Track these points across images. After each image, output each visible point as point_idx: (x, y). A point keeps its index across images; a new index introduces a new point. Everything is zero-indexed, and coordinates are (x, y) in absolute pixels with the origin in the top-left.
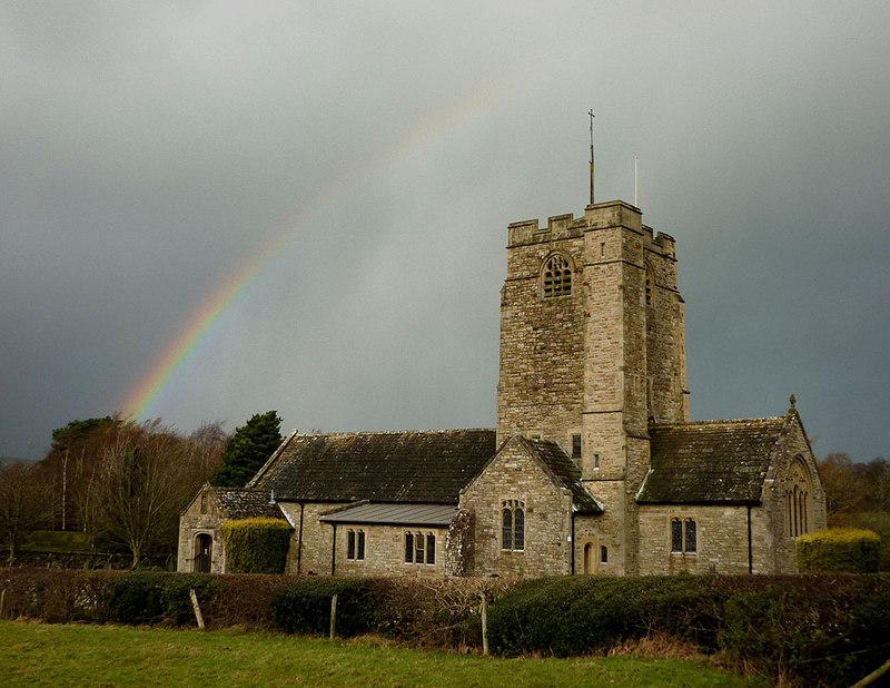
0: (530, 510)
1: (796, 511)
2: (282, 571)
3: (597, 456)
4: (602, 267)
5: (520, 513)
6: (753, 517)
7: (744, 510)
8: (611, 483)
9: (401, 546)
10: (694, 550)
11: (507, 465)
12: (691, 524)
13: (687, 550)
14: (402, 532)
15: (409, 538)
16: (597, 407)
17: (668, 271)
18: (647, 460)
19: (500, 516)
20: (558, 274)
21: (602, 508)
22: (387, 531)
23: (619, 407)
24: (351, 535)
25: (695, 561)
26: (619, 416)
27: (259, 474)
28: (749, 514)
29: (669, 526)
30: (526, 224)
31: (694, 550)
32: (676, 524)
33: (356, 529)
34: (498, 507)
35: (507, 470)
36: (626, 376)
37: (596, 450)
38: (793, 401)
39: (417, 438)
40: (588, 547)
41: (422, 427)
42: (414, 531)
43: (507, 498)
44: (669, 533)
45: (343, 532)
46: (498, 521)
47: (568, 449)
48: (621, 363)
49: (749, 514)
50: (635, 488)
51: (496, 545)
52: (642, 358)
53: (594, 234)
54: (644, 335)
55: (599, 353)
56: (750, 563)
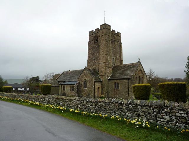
1: (140, 81)
2: (185, 85)
5: (86, 81)
6: (129, 82)
7: (127, 80)
9: (70, 88)
10: (118, 88)
14: (70, 86)
15: (71, 86)
16: (101, 62)
17: (119, 39)
18: (111, 72)
20: (96, 39)
22: (68, 86)
24: (63, 86)
28: (128, 81)
29: (114, 84)
33: (64, 85)
34: (83, 81)
37: (101, 70)
38: (139, 59)
39: (73, 71)
40: (99, 88)
41: (80, 69)
42: (71, 85)
43: (84, 79)
45: (62, 86)
46: (83, 83)
47: (97, 70)
49: (128, 81)
50: (108, 77)
51: (83, 87)
56: (128, 91)
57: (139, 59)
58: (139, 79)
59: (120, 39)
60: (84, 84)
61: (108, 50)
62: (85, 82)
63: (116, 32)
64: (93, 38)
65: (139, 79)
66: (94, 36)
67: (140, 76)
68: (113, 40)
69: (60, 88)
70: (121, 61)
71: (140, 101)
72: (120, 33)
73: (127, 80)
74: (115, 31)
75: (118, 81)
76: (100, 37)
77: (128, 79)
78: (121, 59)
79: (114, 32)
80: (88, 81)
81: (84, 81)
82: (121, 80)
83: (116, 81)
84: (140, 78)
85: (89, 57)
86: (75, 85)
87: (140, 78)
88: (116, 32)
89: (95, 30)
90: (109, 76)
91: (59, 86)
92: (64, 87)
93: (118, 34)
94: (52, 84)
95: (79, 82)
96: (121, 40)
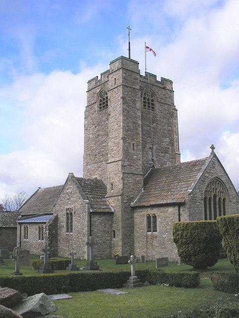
0: (75, 213)
1: (215, 208)
3: (112, 184)
4: (115, 90)
5: (71, 213)
7: (177, 208)
8: (116, 198)
9: (37, 232)
10: (156, 231)
11: (68, 191)
12: (155, 217)
13: (154, 231)
16: (113, 160)
19: (65, 217)
20: (104, 99)
21: (113, 211)
23: (120, 158)
25: (156, 237)
26: (120, 163)
27: (90, 257)
29: (145, 218)
30: (93, 80)
31: (156, 231)
32: (149, 218)
34: (65, 212)
35: (67, 194)
36: (124, 142)
38: (213, 148)
43: (68, 207)
44: (145, 222)
48: (121, 136)
50: (131, 200)
51: (64, 230)
52: (137, 134)
53: (111, 75)
54: (140, 122)
55: (114, 133)
57: (213, 148)
58: (212, 203)
59: (171, 98)
60: (68, 220)
61: (131, 125)
62: (69, 215)
63: (159, 79)
64: (95, 95)
65: (212, 203)
66: (98, 91)
67: (215, 196)
68: (148, 99)
69: (18, 232)
70: (176, 155)
71: (177, 262)
72: (171, 82)
73: (177, 208)
74: (155, 76)
75: (155, 211)
76: (109, 95)
77: (180, 205)
78: (173, 150)
79: (153, 80)
80: (75, 213)
81: (67, 214)
82: (162, 209)
83: (151, 212)
84: (217, 200)
85: (87, 148)
86: (45, 223)
87: (217, 200)
88: (159, 79)
89: (101, 75)
90: (133, 198)
91: (16, 228)
92: (26, 229)
93: (165, 86)
94: (37, 230)
95: (55, 215)
96: (173, 100)
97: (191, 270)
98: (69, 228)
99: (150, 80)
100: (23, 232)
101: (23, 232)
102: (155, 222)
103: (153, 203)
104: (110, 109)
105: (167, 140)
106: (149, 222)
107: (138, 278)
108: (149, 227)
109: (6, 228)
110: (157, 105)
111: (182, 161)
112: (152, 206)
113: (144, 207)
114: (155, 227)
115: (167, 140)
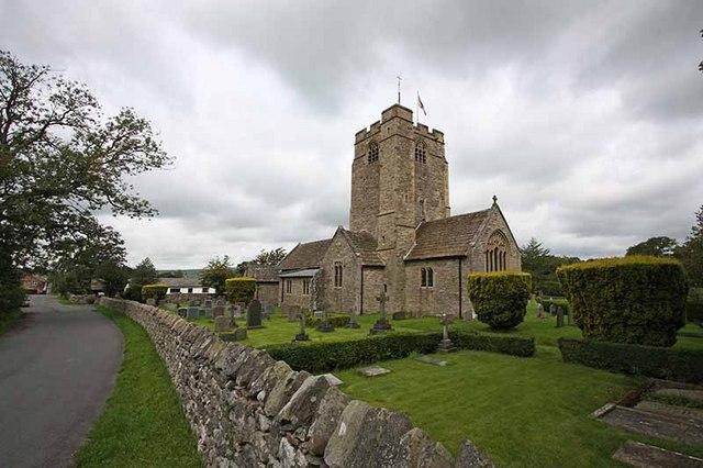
7: (457, 261)
12: (431, 271)
32: (424, 272)
38: (495, 198)
57: (495, 198)
59: (442, 150)
82: (439, 263)
83: (427, 266)
93: (437, 136)
97: (487, 330)
98: (339, 281)
99: (423, 131)
100: (286, 287)
101: (286, 287)
102: (431, 276)
103: (429, 256)
104: (382, 160)
105: (438, 193)
106: (424, 276)
107: (117, 259)
108: (424, 281)
109: (265, 283)
110: (428, 158)
111: (288, 252)
112: (428, 260)
113: (418, 260)
114: (431, 281)
115: (438, 193)
